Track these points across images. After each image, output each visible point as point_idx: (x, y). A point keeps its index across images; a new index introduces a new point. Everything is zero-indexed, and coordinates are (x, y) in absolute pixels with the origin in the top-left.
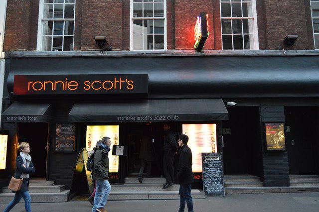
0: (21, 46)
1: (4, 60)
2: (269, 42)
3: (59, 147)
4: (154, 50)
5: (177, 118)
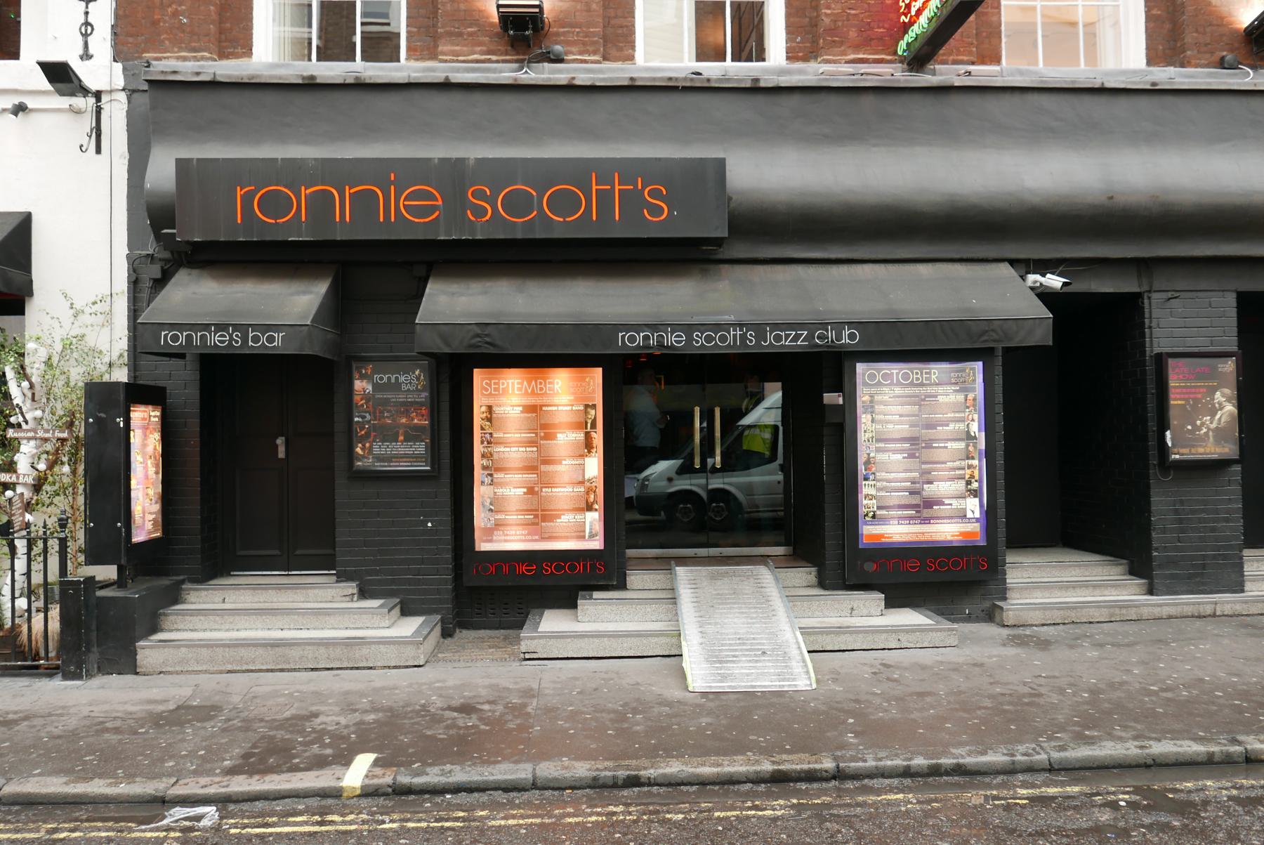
0: (188, 41)
1: (122, 97)
2: (1190, 37)
3: (369, 455)
4: (729, 65)
5: (852, 337)
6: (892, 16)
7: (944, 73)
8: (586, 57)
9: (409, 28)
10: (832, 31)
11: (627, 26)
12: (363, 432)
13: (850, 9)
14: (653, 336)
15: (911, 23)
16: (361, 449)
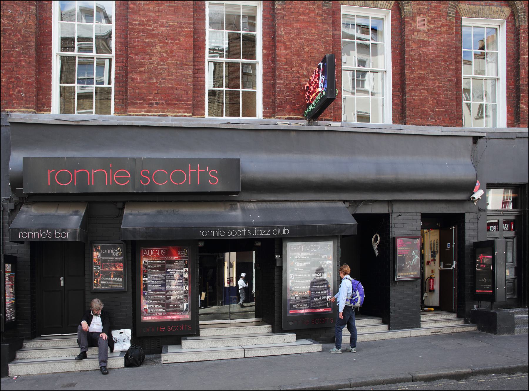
4: (225, 118)
5: (286, 232)
6: (303, 100)
7: (322, 125)
8: (186, 114)
9: (115, 100)
10: (280, 106)
11: (202, 101)
12: (97, 274)
13: (287, 96)
14: (213, 232)
15: (310, 104)
16: (96, 281)
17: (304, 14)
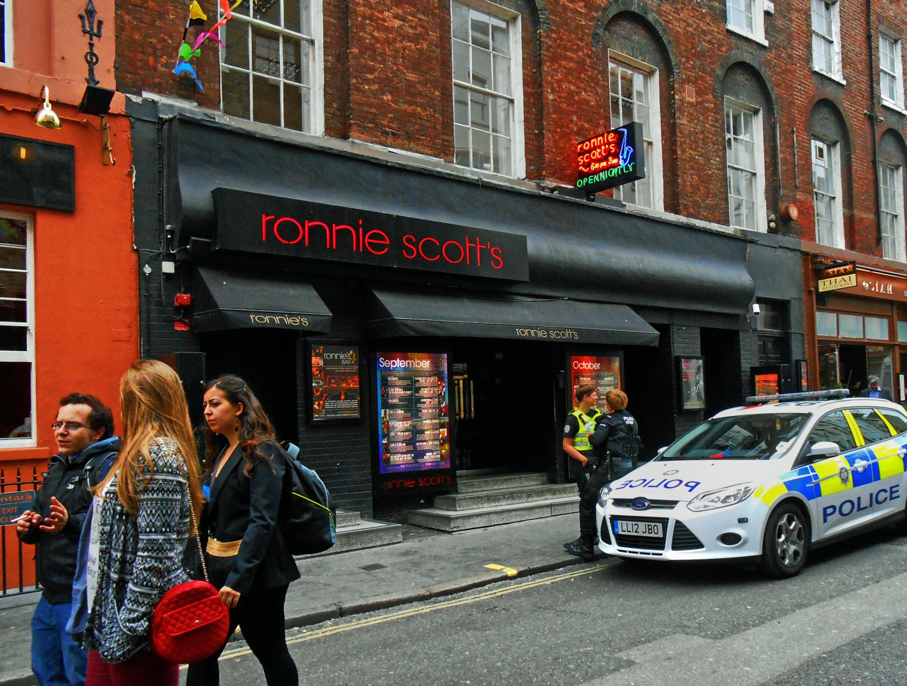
15: (587, 175)
17: (573, 51)
